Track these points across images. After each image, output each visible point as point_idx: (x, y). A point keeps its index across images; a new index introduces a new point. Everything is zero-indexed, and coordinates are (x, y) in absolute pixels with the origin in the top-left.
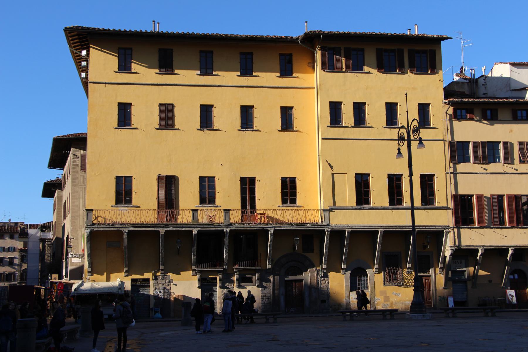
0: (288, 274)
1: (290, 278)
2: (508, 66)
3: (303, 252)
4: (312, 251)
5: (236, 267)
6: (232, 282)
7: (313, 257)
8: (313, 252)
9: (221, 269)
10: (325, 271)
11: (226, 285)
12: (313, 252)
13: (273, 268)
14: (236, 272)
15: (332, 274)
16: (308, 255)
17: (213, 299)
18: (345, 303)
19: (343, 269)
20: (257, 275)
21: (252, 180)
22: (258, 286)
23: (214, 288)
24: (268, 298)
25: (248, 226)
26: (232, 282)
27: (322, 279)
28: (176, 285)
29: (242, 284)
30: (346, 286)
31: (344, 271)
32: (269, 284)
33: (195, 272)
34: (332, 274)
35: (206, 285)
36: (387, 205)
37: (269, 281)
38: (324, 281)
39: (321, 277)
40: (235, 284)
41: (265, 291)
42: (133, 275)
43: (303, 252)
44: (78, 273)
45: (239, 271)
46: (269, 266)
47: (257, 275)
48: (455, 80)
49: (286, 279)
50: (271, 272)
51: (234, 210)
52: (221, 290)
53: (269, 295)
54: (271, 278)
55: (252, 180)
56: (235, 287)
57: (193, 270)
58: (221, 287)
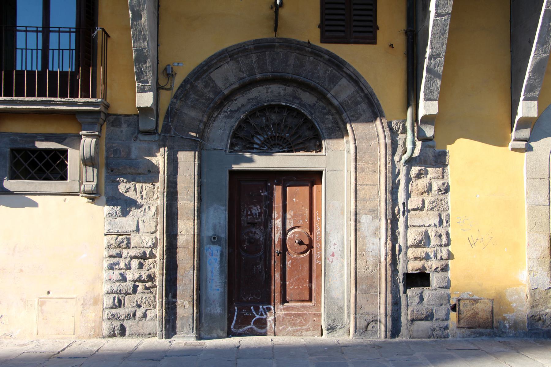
0: (246, 139)
1: (262, 162)
3: (324, 40)
4: (367, 33)
7: (375, 63)
8: (372, 40)
10: (429, 132)
12: (372, 40)
15: (462, 152)
16: (349, 53)
18: (525, 291)
19: (525, 123)
20: (88, 143)
22: (93, 196)
24: (143, 257)
27: (415, 170)
28: (65, 201)
30: (533, 207)
31: (526, 133)
32: (147, 186)
34: (462, 152)
37: (149, 174)
38: (422, 183)
39: (410, 162)
41: (126, 224)
42: (391, 243)
43: (324, 40)
44: (261, 220)
47: (88, 143)
49: (235, 167)
50: (169, 128)
53: (148, 241)
54: (160, 159)
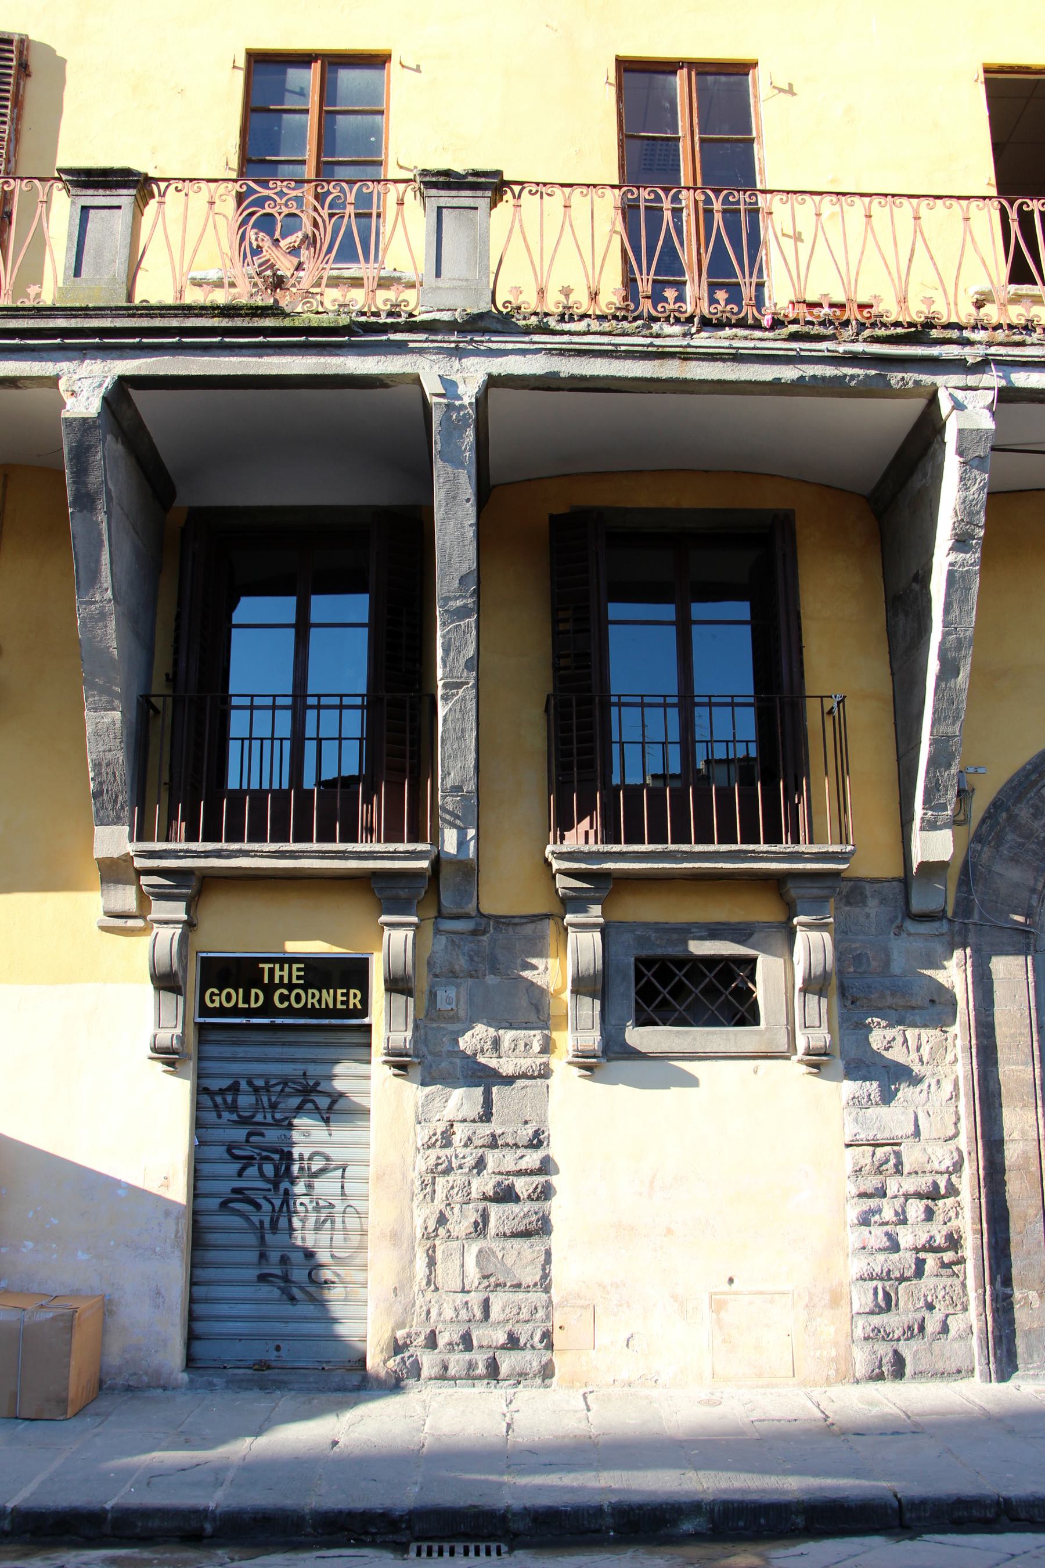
2: (494, 211)
5: (573, 840)
6: (533, 1011)
9: (405, 857)
11: (467, 1042)
13: (969, 871)
14: (574, 902)
17: (988, 1501)
20: (812, 945)
21: (725, 84)
22: (818, 1061)
23: (345, 1076)
25: (704, 340)
26: (533, 1011)
29: (637, 1037)
32: (929, 1036)
33: (126, 898)
35: (255, 1043)
36: (323, 779)
37: (937, 1008)
40: (566, 1041)
41: (893, 1119)
45: (603, 885)
46: (933, 845)
47: (812, 945)
48: (889, 1055)
51: (542, 188)
52: (412, 1092)
54: (954, 974)
55: (725, 84)
56: (560, 1062)
57: (113, 872)
58: (401, 1063)
